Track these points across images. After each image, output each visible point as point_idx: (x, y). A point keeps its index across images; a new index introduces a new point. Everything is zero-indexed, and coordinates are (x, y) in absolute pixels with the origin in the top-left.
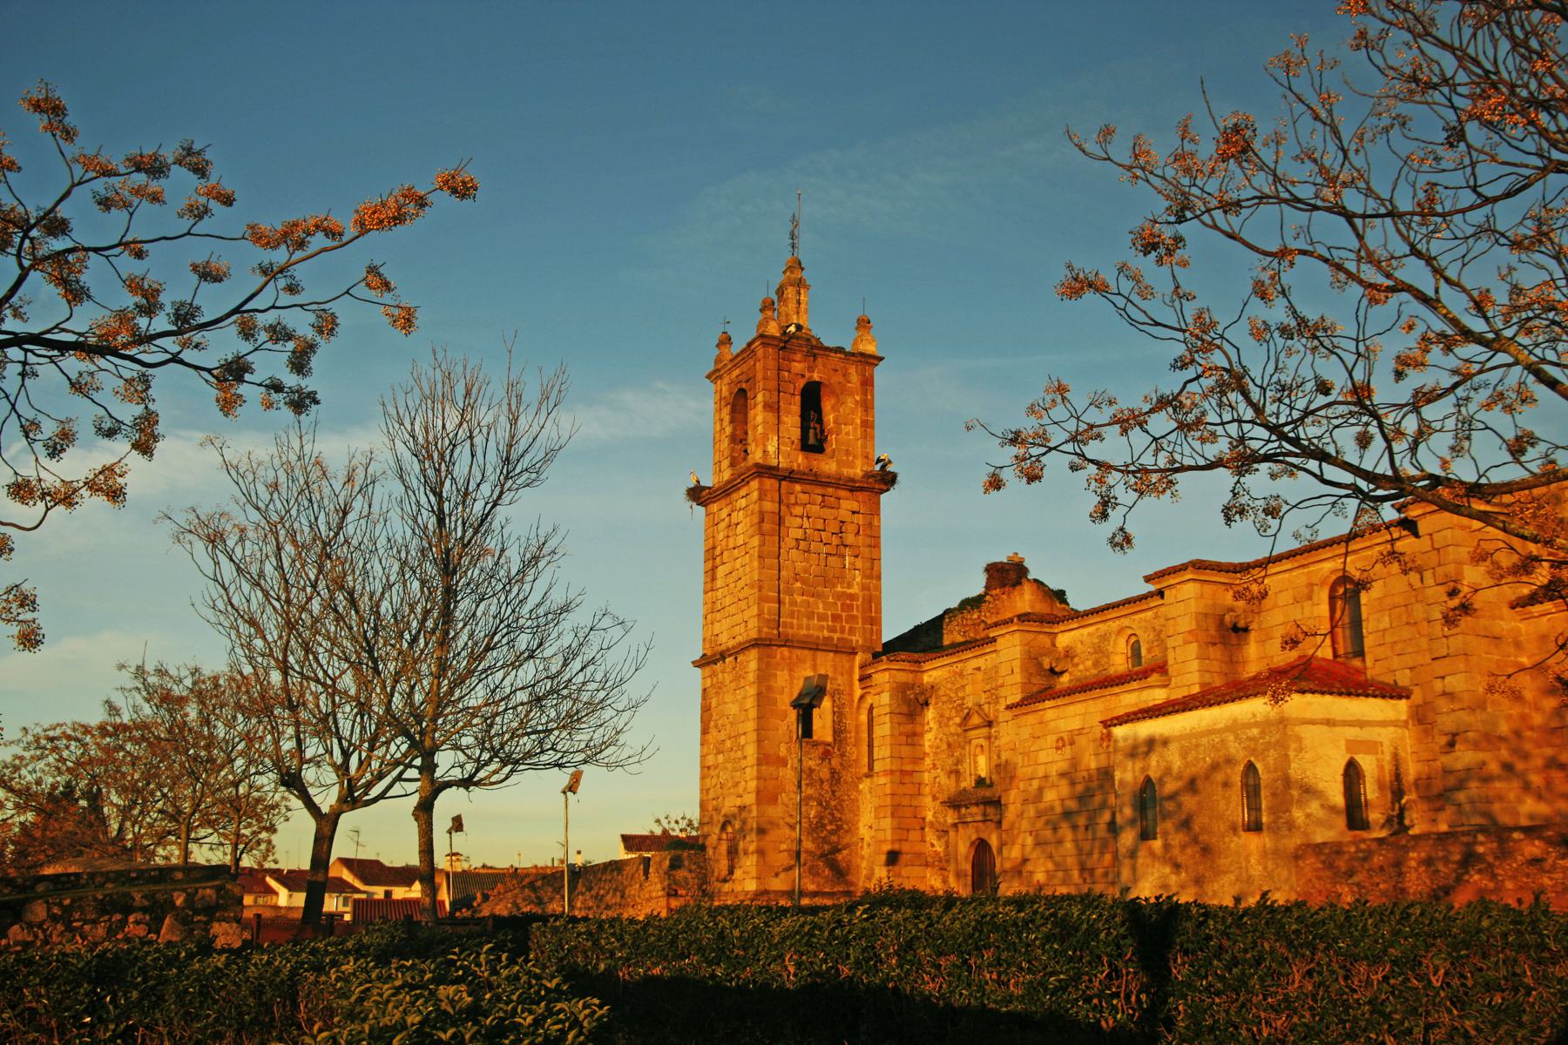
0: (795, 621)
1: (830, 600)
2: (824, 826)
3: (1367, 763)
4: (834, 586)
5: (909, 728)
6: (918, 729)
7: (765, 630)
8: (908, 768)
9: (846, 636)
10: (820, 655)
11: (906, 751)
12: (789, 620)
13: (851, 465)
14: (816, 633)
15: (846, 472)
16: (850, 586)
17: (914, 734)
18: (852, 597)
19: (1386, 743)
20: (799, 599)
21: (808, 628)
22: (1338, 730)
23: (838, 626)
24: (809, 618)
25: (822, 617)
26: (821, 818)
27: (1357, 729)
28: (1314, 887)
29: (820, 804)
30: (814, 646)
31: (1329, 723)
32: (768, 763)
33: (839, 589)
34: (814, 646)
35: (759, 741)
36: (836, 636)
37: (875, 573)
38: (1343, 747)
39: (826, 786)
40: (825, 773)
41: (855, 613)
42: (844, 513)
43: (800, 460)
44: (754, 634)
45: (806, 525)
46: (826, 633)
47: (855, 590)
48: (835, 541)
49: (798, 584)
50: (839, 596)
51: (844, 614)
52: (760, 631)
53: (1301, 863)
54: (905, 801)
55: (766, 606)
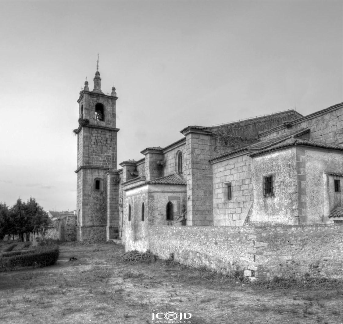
0: (93, 162)
1: (103, 157)
2: (101, 210)
3: (174, 202)
4: (104, 153)
5: (115, 188)
6: (117, 188)
7: (85, 164)
8: (114, 197)
9: (107, 165)
10: (100, 171)
11: (114, 193)
12: (91, 162)
13: (109, 124)
14: (99, 165)
15: (108, 126)
16: (108, 153)
17: (116, 189)
18: (109, 156)
19: (181, 197)
20: (94, 157)
21: (97, 163)
22: (166, 194)
23: (105, 163)
24: (97, 161)
25: (100, 161)
26: (100, 208)
27: (172, 193)
28: (283, 175)
29: (100, 205)
30: (98, 168)
31: (163, 192)
32: (86, 196)
33: (105, 154)
34: (98, 168)
35: (83, 191)
36: (104, 165)
37: (115, 150)
38: (167, 198)
39: (102, 201)
40: (101, 198)
41: (110, 160)
42: (107, 136)
43: (338, 178)
44: (82, 165)
45: (97, 139)
46: (102, 165)
47: (110, 154)
48: (105, 143)
49: (94, 153)
50: (105, 156)
51: (107, 160)
52: (83, 164)
53: (208, 208)
54: (114, 205)
55: (85, 158)
